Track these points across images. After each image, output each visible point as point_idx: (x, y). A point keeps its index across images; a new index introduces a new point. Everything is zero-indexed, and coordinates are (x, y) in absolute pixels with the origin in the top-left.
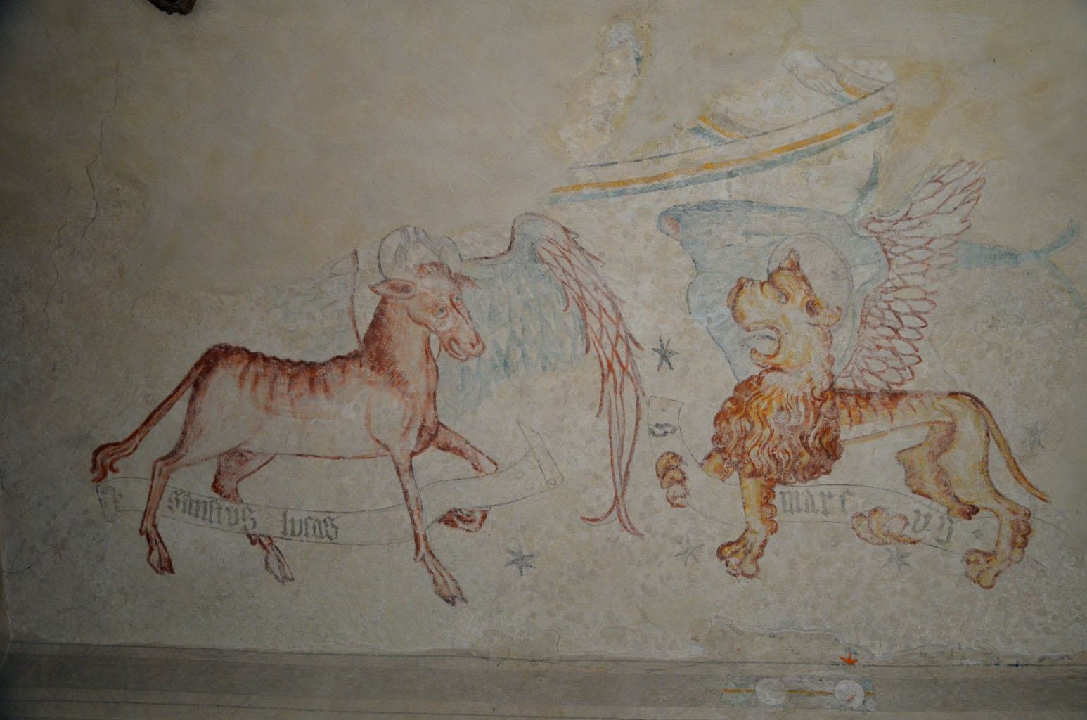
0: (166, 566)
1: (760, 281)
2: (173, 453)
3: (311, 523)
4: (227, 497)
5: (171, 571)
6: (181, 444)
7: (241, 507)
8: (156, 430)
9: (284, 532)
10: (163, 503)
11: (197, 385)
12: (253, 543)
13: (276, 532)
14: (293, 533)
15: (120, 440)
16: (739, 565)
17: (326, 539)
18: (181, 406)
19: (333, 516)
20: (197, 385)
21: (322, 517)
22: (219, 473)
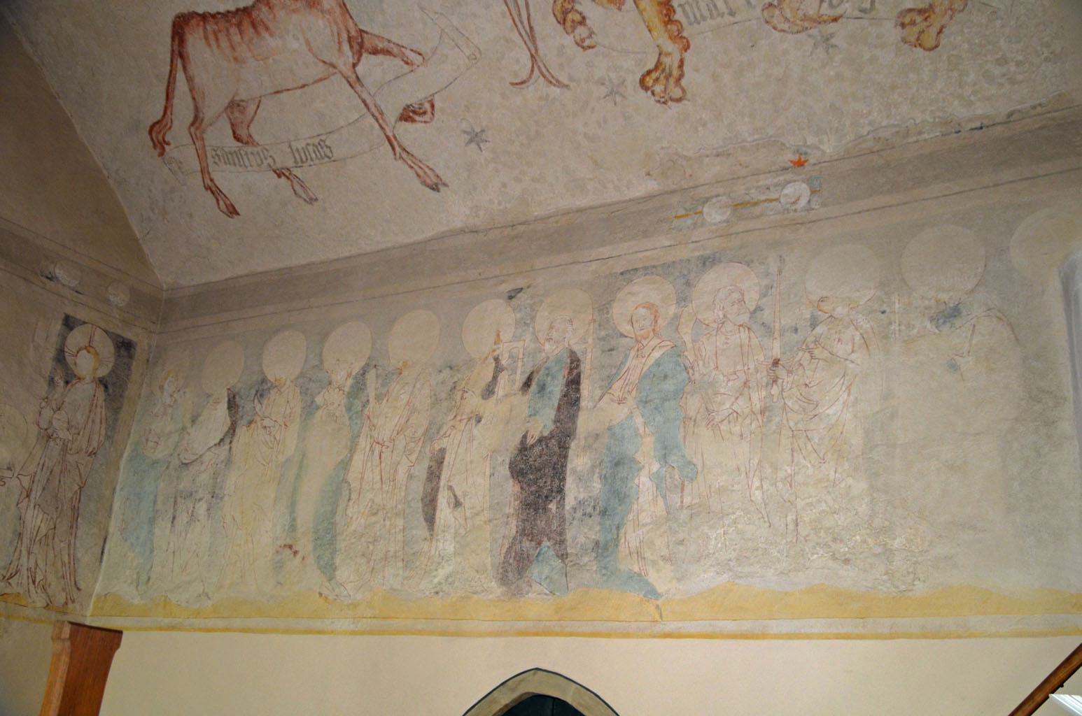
0: (232, 211)
2: (196, 118)
3: (310, 148)
4: (247, 143)
5: (238, 214)
6: (197, 109)
7: (259, 149)
9: (296, 162)
10: (210, 161)
11: (181, 56)
12: (279, 176)
13: (290, 164)
15: (159, 117)
17: (327, 159)
18: (180, 76)
19: (323, 138)
20: (181, 56)
21: (316, 141)
22: (232, 125)
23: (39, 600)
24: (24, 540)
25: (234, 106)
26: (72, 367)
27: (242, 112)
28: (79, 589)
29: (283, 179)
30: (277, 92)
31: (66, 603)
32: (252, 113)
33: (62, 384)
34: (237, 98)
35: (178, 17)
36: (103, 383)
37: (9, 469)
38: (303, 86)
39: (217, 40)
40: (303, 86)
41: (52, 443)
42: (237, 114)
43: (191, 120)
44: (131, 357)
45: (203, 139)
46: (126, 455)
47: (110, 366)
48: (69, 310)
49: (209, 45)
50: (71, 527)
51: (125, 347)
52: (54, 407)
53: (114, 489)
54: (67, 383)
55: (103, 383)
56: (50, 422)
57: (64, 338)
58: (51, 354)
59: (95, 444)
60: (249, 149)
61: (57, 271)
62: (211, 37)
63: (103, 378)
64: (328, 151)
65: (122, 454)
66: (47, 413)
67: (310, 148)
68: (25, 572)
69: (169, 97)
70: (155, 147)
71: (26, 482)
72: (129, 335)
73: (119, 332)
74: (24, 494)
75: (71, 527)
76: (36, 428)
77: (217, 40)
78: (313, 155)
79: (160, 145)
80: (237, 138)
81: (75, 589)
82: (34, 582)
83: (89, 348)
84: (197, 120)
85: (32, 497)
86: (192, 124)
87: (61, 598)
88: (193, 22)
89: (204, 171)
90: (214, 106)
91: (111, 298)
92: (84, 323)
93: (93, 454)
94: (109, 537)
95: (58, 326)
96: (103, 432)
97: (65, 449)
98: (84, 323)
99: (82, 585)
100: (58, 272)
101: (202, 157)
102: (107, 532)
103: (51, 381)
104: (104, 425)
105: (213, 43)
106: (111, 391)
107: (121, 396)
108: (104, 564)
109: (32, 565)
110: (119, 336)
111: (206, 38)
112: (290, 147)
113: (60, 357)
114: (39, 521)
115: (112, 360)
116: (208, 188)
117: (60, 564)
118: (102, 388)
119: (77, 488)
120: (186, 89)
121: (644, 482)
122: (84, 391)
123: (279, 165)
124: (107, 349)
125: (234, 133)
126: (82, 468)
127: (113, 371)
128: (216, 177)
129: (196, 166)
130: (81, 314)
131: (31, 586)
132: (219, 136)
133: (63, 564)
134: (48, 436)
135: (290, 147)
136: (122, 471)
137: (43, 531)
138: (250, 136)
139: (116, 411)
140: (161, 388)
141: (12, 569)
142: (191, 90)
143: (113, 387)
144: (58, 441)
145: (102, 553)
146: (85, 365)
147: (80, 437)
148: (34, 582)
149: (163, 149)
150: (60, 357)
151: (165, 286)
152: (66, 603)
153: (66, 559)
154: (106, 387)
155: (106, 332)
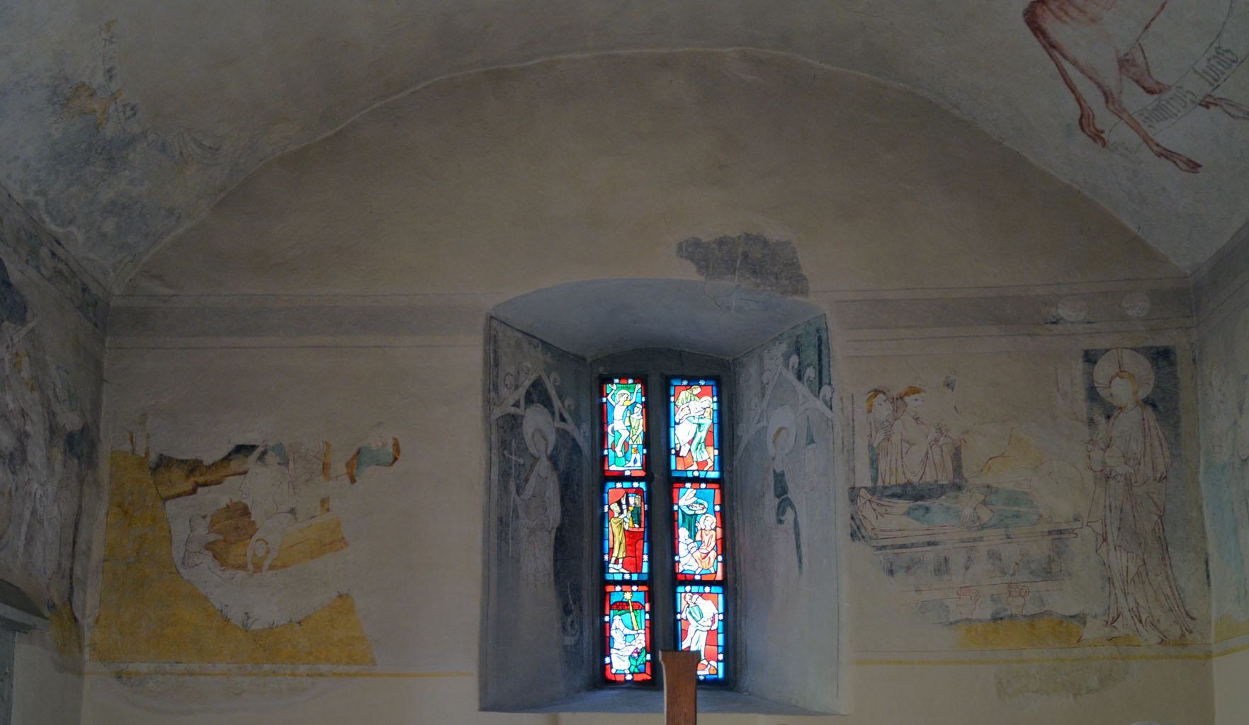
0: (1194, 166)
1: (662, 375)
2: (1105, 94)
3: (1213, 62)
4: (1161, 91)
5: (1200, 166)
6: (1100, 86)
7: (1173, 89)
8: (1080, 89)
9: (1211, 84)
10: (1145, 127)
11: (1053, 47)
12: (1208, 107)
13: (1209, 89)
14: (1216, 80)
15: (1079, 112)
16: (575, 645)
17: (1235, 65)
18: (1066, 65)
19: (1216, 45)
20: (1053, 47)
21: (1213, 52)
22: (1137, 82)
23: (1154, 638)
24: (1117, 584)
25: (1125, 63)
26: (1109, 399)
27: (1134, 65)
28: (1192, 618)
29: (1213, 108)
30: (1146, 28)
31: (1183, 635)
32: (1142, 59)
33: (1102, 420)
34: (1121, 54)
35: (1025, 15)
36: (1150, 403)
37: (1076, 520)
38: (1163, 7)
39: (1066, 13)
40: (1163, 7)
41: (1112, 482)
42: (1133, 70)
43: (1103, 99)
44: (1172, 364)
45: (1124, 110)
46: (1201, 469)
47: (1152, 383)
48: (1087, 344)
49: (1065, 22)
50: (1163, 558)
51: (1162, 356)
52: (1102, 445)
53: (1201, 507)
54: (1108, 417)
55: (1150, 403)
56: (1104, 462)
57: (1090, 375)
58: (1081, 395)
59: (1161, 468)
60: (1168, 95)
61: (1060, 311)
62: (1061, 14)
63: (1148, 398)
64: (1229, 55)
65: (1198, 468)
66: (1097, 455)
67: (1213, 62)
68: (1127, 614)
69: (1073, 90)
70: (1095, 141)
71: (1098, 527)
72: (1162, 341)
73: (1150, 343)
74: (1100, 540)
75: (1163, 558)
76: (1091, 473)
77: (1066, 13)
78: (1221, 68)
79: (1097, 136)
80: (1150, 92)
81: (1188, 620)
82: (1140, 621)
83: (1121, 373)
84: (1107, 96)
85: (1110, 538)
86: (1107, 101)
87: (1175, 631)
88: (1038, 11)
89: (1147, 140)
90: (1110, 76)
91: (1129, 312)
92: (1107, 350)
93: (1164, 478)
94: (1210, 559)
95: (1079, 366)
96: (1167, 453)
97: (1129, 484)
98: (1107, 350)
99: (1195, 614)
100: (1063, 312)
101: (1136, 128)
102: (1207, 554)
103: (1091, 422)
104: (1165, 445)
105: (1065, 18)
106: (1161, 407)
107: (1176, 409)
108: (1213, 587)
109: (1132, 605)
110: (1151, 348)
111: (1058, 17)
112: (1196, 72)
113: (1093, 394)
114: (1124, 560)
115: (1152, 375)
116: (1160, 155)
117: (1163, 598)
118: (1149, 409)
119: (1156, 518)
120: (1079, 74)
121: (21, 549)
122: (1130, 420)
123: (1200, 98)
124: (1142, 367)
125: (1144, 88)
126: (1155, 497)
127: (1156, 387)
128: (1158, 139)
129: (1137, 139)
130: (1099, 344)
131: (1139, 625)
132: (1135, 99)
133: (1167, 597)
134: (1106, 477)
135: (1196, 72)
136: (1203, 485)
137: (1133, 570)
138: (1158, 83)
139: (1176, 426)
140: (1211, 384)
141: (1113, 613)
142: (1082, 71)
143: (1163, 404)
144: (1119, 478)
145: (1208, 576)
146: (1122, 392)
147: (1142, 467)
148: (1140, 621)
149: (1102, 139)
150: (1093, 394)
151: (1189, 273)
152: (1183, 635)
153: (1169, 591)
154: (1154, 406)
155: (1135, 350)
